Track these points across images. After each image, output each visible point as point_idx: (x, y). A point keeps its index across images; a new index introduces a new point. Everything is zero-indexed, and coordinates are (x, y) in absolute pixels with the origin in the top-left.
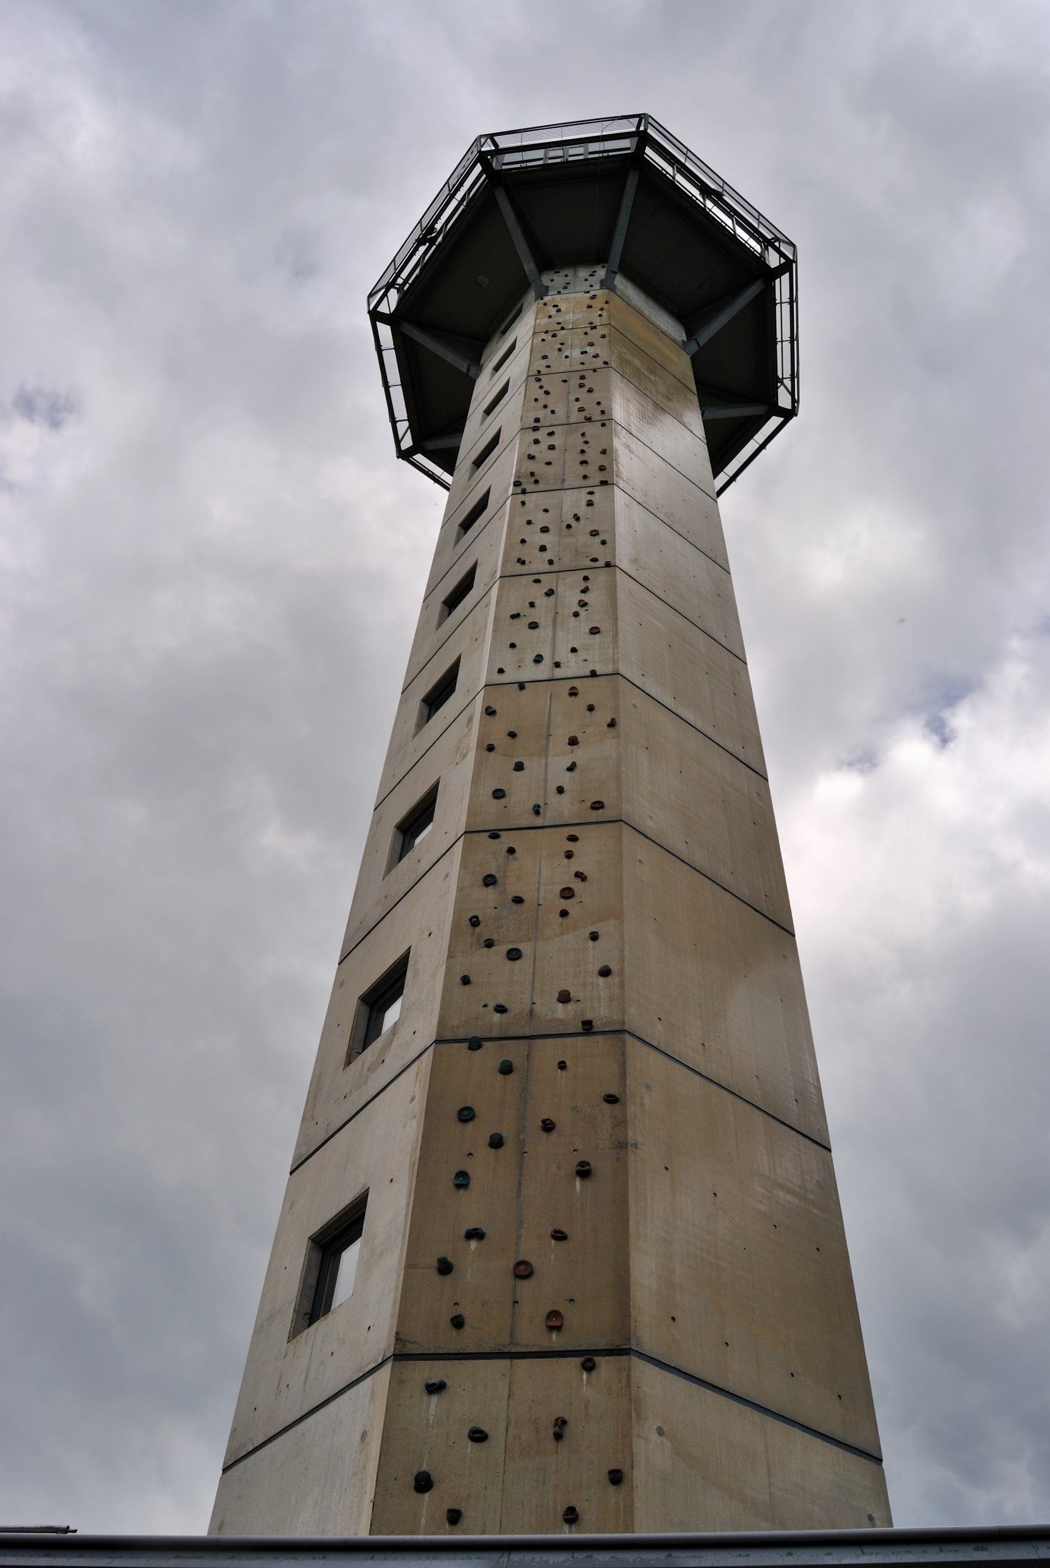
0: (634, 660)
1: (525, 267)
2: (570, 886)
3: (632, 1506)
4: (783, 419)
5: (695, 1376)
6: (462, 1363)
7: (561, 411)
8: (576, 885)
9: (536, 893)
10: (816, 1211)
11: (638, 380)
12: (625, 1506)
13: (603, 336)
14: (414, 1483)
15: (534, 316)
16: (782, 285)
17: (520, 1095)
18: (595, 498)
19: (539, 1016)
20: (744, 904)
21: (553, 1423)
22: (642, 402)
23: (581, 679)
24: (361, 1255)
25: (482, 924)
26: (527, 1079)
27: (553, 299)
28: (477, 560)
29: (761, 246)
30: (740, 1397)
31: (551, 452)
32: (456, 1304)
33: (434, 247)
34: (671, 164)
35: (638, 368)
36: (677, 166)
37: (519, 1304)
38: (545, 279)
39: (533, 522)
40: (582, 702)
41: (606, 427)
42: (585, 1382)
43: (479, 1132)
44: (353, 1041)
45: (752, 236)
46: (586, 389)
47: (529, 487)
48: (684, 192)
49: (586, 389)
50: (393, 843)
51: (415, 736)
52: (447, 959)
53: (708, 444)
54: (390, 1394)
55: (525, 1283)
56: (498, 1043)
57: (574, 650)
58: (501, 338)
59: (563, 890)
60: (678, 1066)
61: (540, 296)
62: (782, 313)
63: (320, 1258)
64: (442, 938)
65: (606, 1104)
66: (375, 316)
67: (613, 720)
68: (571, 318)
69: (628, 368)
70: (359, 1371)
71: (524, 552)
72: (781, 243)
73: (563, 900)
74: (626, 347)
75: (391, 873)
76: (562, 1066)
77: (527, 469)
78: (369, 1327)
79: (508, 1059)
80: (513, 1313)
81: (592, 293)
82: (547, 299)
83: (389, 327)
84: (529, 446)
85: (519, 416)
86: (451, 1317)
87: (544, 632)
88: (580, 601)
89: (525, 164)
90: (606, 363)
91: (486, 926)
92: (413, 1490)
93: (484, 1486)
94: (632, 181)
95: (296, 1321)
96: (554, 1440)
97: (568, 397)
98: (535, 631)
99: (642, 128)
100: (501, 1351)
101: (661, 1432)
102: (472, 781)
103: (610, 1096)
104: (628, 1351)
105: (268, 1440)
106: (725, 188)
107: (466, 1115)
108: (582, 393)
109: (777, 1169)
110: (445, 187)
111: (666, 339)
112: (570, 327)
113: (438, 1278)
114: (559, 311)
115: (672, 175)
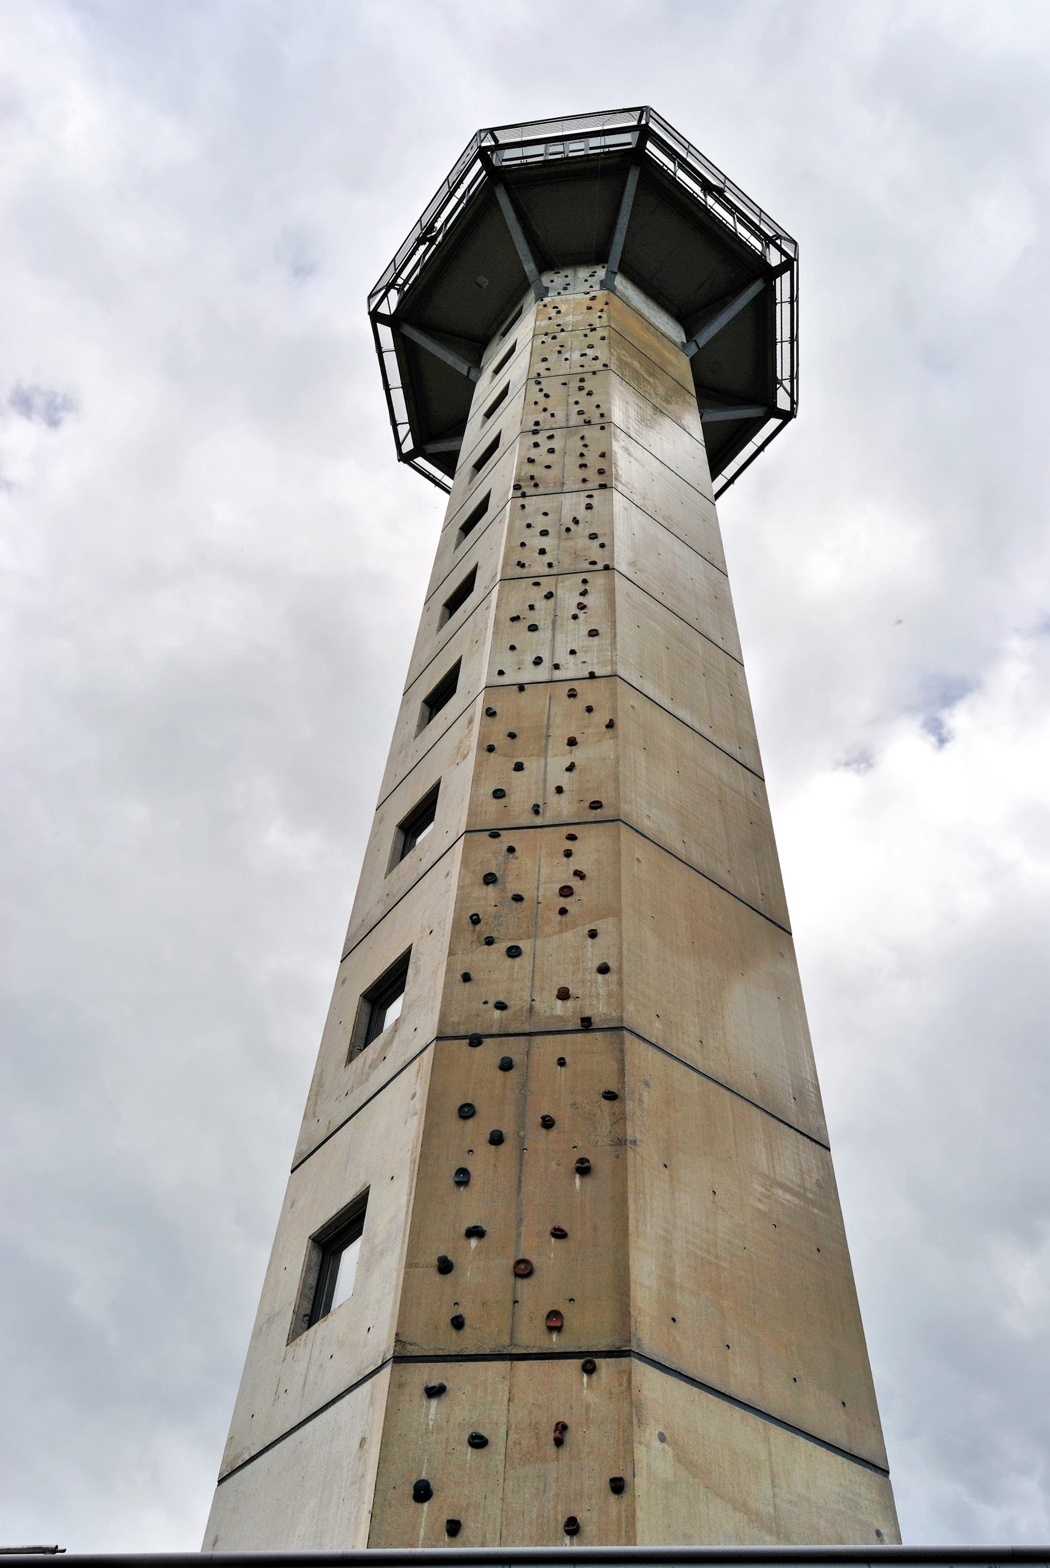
0: (632, 661)
1: (525, 267)
2: (569, 884)
3: (634, 1517)
4: (782, 421)
5: (697, 1379)
6: (462, 1365)
7: (560, 414)
8: (575, 883)
9: (535, 892)
10: (815, 1211)
11: (636, 382)
12: (627, 1517)
13: (603, 338)
14: (413, 1492)
15: (534, 318)
16: (782, 285)
17: (520, 1092)
18: (594, 502)
19: (538, 1013)
20: (741, 903)
21: (553, 1427)
22: (641, 405)
23: (581, 681)
24: (362, 1255)
25: (482, 922)
26: (527, 1076)
27: (553, 300)
28: (478, 563)
29: (762, 244)
30: (742, 1403)
31: (551, 455)
32: (456, 1304)
33: (434, 246)
34: (673, 160)
35: (637, 371)
36: (678, 162)
37: (519, 1303)
38: (545, 280)
39: (533, 526)
40: (580, 703)
41: (605, 430)
42: (585, 1385)
43: (478, 1130)
44: (355, 1038)
45: (753, 233)
46: (585, 392)
47: (529, 491)
48: (685, 188)
49: (585, 392)
50: (395, 842)
51: (416, 737)
52: (448, 956)
53: (706, 447)
54: (389, 1398)
55: (525, 1282)
56: (498, 1039)
57: (573, 652)
58: (501, 340)
59: (562, 889)
60: (676, 1063)
61: (540, 298)
62: (783, 313)
63: (321, 1258)
64: (443, 935)
65: (604, 1100)
66: (376, 317)
67: (611, 721)
68: (571, 320)
69: (628, 370)
70: (359, 1374)
71: (525, 556)
72: (782, 240)
73: (562, 898)
74: (625, 350)
75: (393, 871)
76: (562, 1062)
77: (526, 473)
78: (369, 1329)
79: (508, 1056)
80: (514, 1313)
81: (592, 294)
82: (546, 300)
83: (420, 457)
84: (528, 449)
85: (519, 420)
86: (451, 1317)
87: (544, 634)
88: (579, 604)
89: (525, 160)
90: (605, 365)
91: (486, 924)
92: (412, 1500)
93: (484, 1495)
94: (633, 178)
95: (295, 1323)
96: (554, 1445)
97: (568, 400)
98: (535, 634)
99: (643, 122)
100: (501, 1353)
101: (662, 1438)
102: (473, 780)
103: (609, 1092)
104: (628, 1353)
105: (265, 1448)
106: (726, 184)
107: (467, 1112)
108: (581, 396)
109: (776, 1168)
110: (445, 184)
111: (665, 340)
112: (570, 329)
113: (438, 1278)
114: (559, 312)
115: (673, 170)
